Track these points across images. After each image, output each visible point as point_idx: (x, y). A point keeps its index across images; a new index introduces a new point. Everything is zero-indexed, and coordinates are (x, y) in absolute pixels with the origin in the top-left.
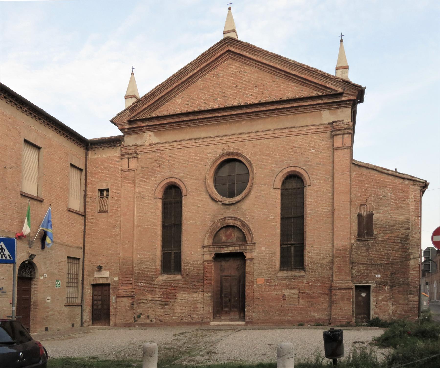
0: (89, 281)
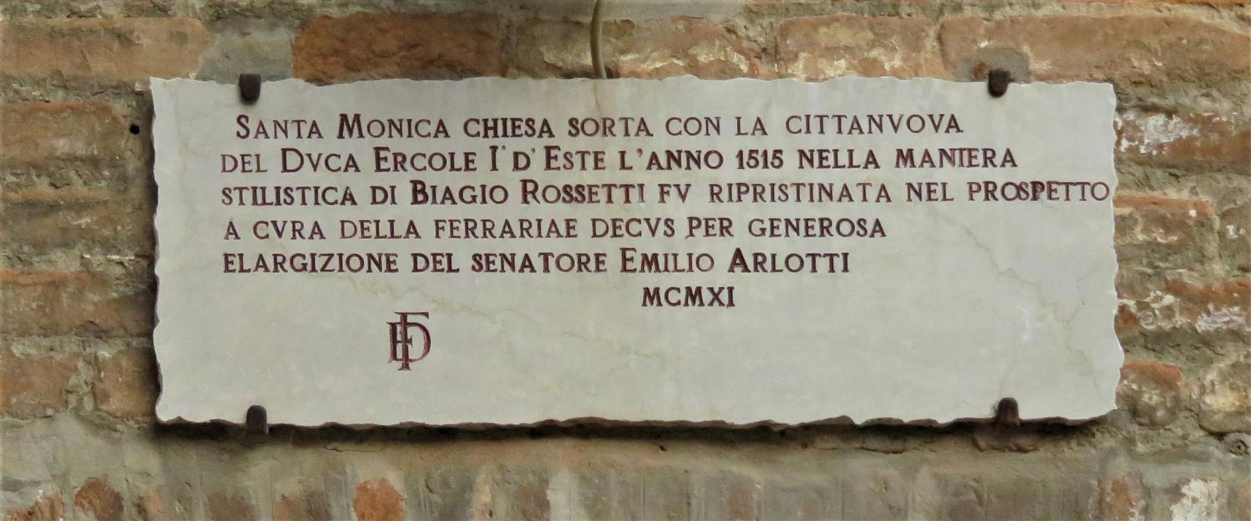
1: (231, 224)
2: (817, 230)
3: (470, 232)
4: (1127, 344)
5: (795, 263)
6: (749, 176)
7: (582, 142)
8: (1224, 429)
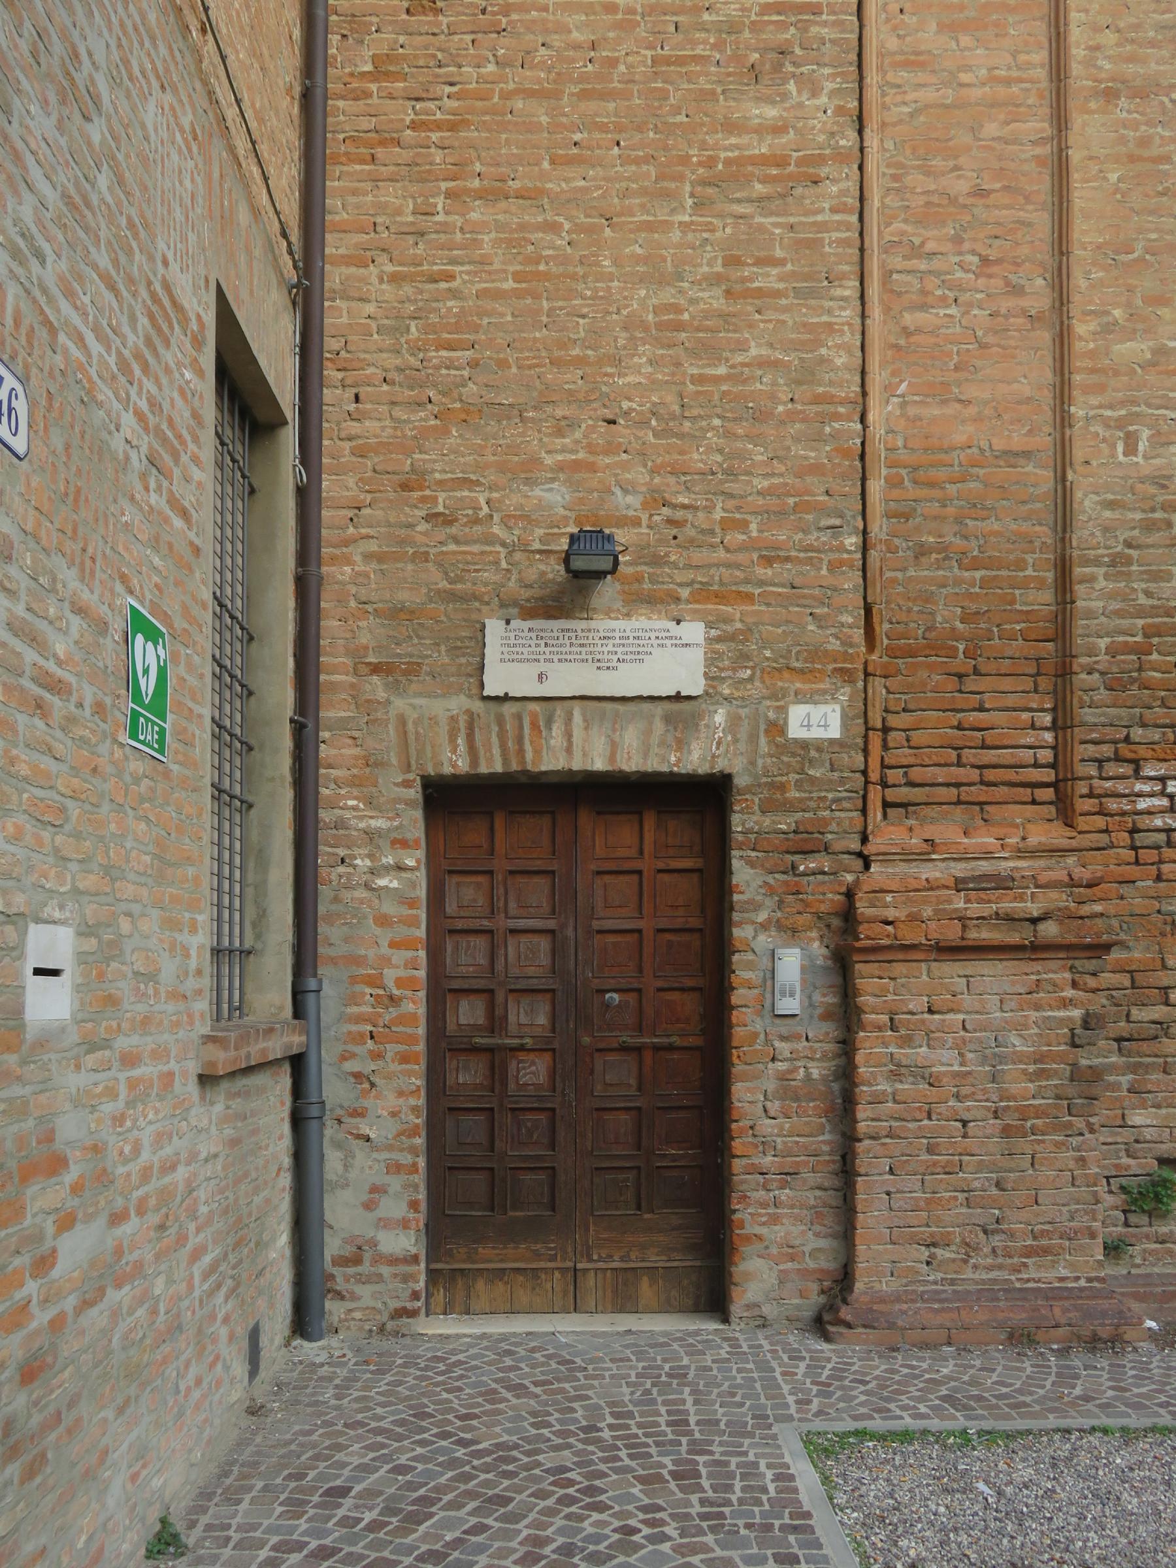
0: (394, 738)
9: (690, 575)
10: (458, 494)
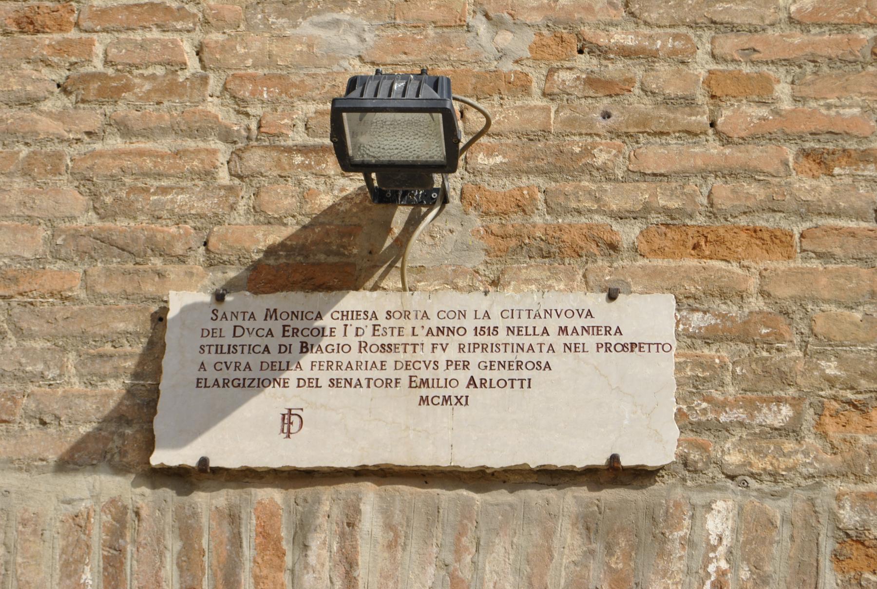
1: (203, 364)
2: (515, 367)
3: (329, 367)
4: (682, 429)
5: (502, 383)
6: (480, 339)
7: (392, 322)
8: (735, 474)
9: (643, 193)
10: (137, 36)
